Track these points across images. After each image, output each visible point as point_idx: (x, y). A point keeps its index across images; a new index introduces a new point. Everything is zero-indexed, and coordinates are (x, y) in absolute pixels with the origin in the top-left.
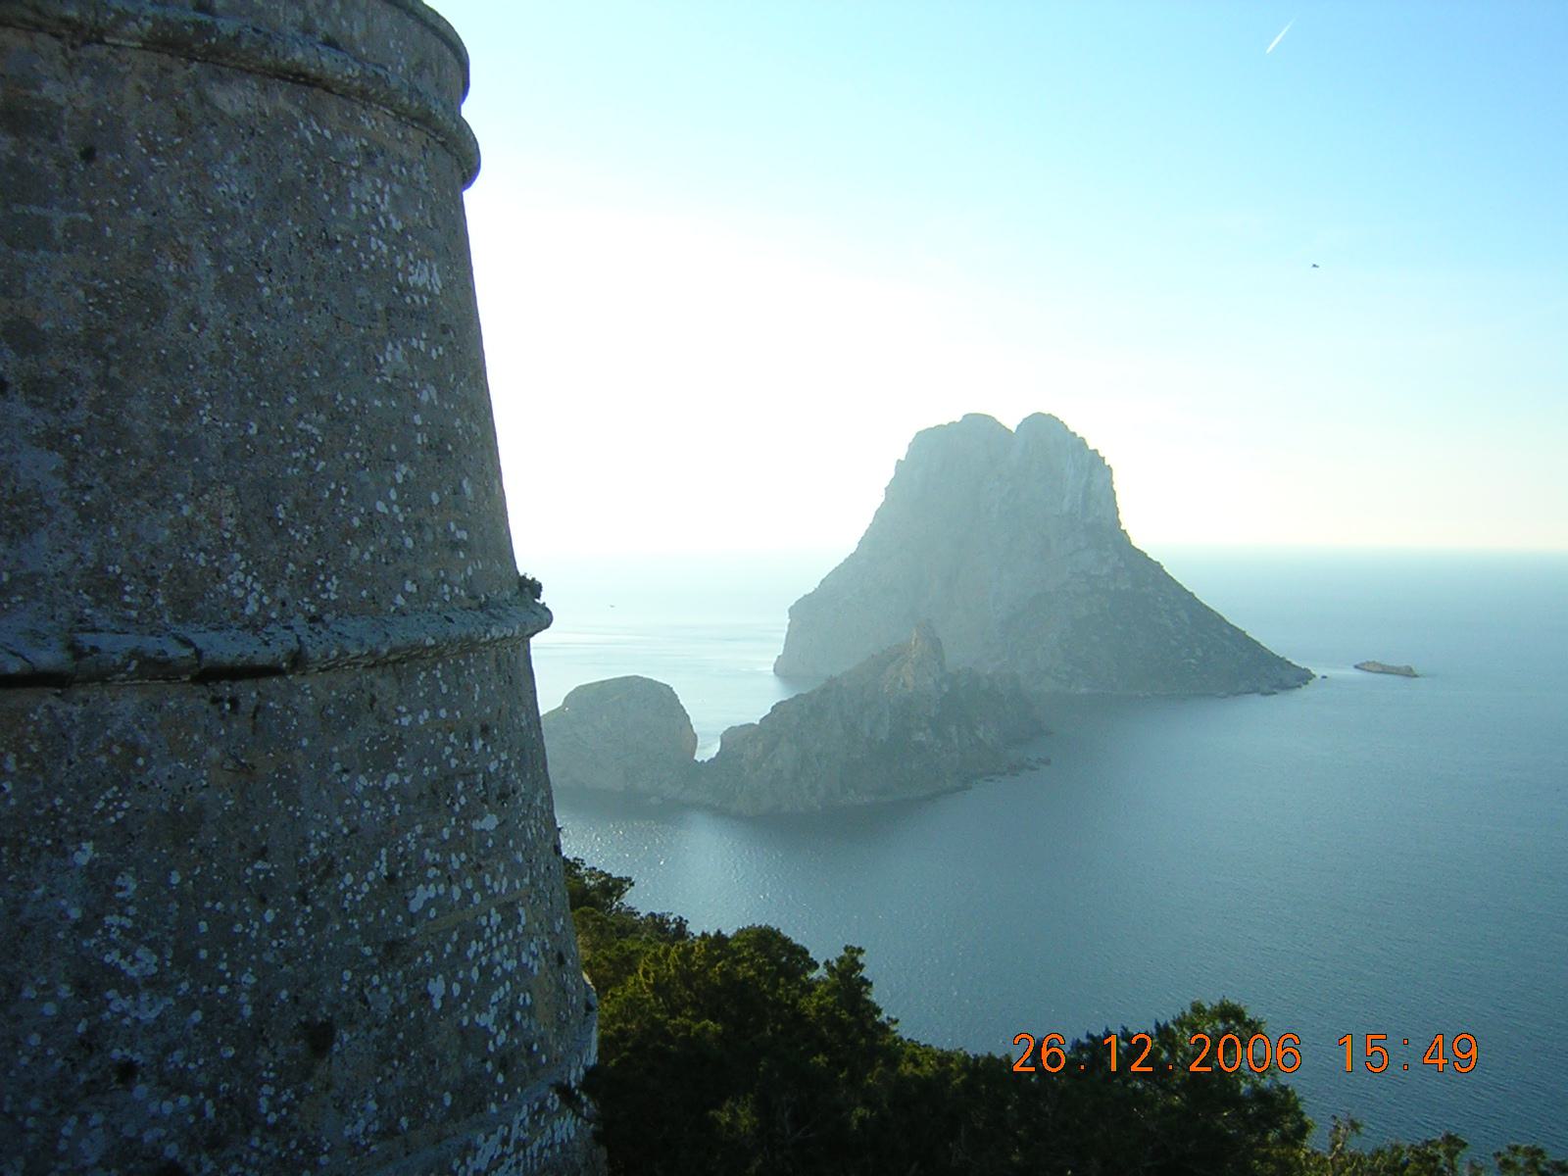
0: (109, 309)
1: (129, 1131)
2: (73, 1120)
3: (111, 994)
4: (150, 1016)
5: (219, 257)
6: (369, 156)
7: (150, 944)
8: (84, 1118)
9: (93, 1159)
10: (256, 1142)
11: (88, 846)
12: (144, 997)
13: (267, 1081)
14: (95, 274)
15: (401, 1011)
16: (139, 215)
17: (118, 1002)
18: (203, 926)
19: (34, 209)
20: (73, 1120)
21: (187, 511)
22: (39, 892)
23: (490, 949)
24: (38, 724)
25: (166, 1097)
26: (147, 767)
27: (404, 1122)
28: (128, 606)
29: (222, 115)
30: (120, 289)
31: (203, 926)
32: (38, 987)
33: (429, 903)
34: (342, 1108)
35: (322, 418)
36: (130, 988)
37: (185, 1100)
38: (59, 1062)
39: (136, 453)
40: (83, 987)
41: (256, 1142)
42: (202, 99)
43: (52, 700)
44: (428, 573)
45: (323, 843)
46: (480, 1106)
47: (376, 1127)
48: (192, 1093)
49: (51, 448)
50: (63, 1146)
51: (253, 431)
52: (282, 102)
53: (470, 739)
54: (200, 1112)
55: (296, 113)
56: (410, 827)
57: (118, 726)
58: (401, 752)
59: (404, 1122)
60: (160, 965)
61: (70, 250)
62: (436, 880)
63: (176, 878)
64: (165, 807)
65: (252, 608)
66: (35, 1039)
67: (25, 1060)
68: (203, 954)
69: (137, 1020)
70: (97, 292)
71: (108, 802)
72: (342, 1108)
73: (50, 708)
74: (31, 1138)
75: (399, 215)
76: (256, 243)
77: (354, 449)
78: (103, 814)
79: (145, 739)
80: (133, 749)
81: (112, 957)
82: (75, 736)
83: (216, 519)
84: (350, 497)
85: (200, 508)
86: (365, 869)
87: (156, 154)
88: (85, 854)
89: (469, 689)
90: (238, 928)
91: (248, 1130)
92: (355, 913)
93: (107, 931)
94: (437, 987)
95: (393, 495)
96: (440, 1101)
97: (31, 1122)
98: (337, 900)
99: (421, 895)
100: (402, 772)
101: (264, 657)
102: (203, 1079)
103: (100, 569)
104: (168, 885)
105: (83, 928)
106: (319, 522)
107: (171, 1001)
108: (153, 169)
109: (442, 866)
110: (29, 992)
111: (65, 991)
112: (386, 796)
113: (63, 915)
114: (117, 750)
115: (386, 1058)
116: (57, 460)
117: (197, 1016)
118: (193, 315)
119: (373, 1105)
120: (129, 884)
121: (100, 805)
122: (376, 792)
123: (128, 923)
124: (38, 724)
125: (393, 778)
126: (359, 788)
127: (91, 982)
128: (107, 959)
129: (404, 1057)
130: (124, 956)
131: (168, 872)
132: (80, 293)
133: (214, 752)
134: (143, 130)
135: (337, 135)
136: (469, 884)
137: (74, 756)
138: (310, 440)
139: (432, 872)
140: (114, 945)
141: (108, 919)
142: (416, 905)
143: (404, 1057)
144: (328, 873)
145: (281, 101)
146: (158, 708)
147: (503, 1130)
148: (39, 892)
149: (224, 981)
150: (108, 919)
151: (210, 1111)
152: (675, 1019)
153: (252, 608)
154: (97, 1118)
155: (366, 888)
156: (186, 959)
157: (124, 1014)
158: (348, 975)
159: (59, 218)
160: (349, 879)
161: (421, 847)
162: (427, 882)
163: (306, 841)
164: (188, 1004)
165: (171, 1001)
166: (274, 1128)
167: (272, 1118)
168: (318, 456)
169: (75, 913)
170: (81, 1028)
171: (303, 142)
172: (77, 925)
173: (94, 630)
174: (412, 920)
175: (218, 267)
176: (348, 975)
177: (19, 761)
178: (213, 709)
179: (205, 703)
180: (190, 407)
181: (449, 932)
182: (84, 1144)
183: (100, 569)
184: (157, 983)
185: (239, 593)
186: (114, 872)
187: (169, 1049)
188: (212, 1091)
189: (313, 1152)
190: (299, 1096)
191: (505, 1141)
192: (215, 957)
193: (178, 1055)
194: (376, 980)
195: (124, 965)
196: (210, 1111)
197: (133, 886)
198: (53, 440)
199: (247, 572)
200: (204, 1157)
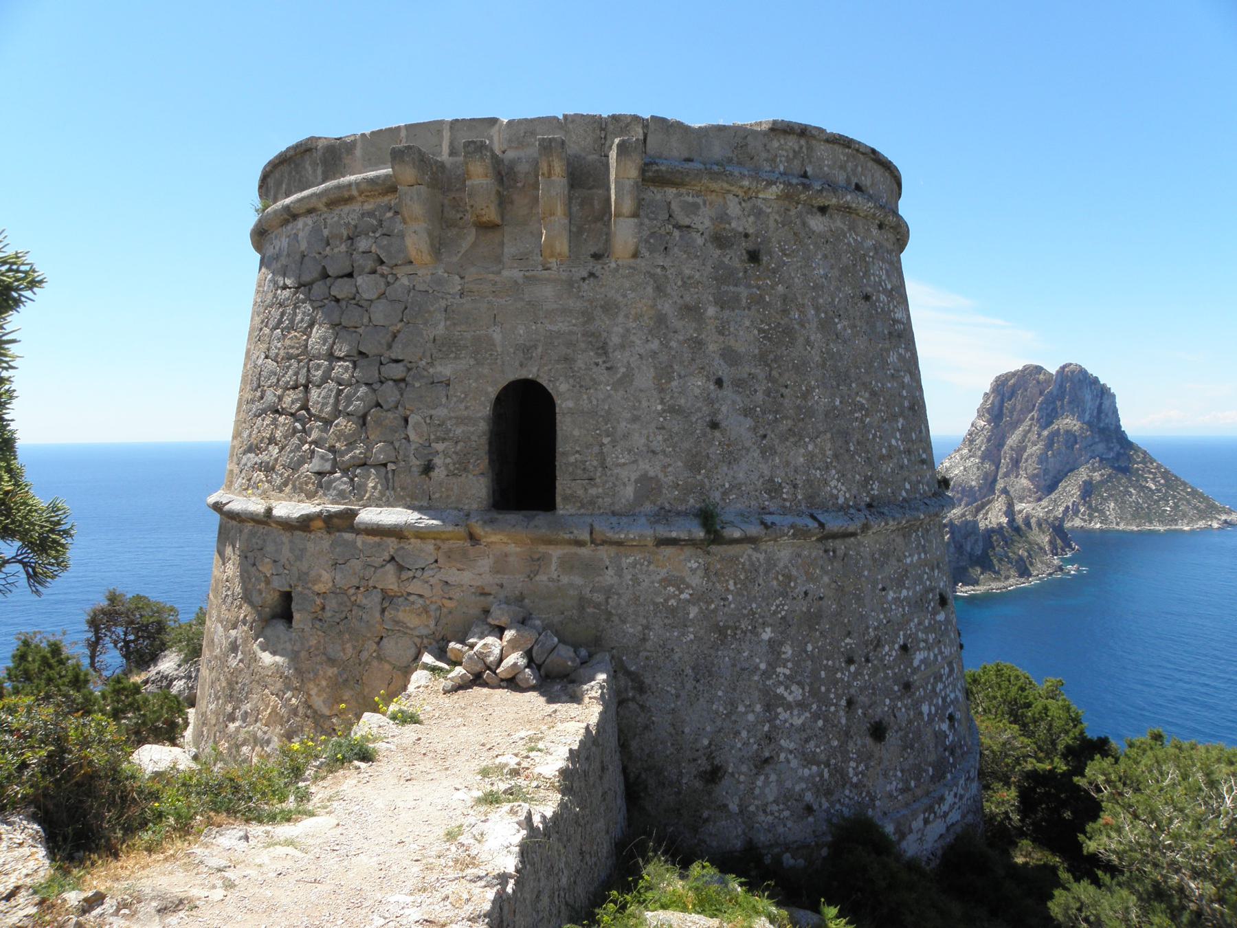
0: (770, 340)
1: (788, 784)
2: (762, 778)
3: (780, 710)
4: (798, 722)
5: (818, 309)
6: (875, 249)
7: (799, 683)
8: (767, 777)
9: (771, 799)
10: (847, 792)
11: (768, 630)
12: (796, 712)
13: (852, 759)
14: (762, 321)
15: (910, 722)
16: (780, 288)
17: (783, 715)
18: (823, 674)
19: (732, 288)
20: (762, 778)
21: (810, 447)
22: (745, 654)
23: (945, 687)
24: (743, 564)
25: (804, 767)
26: (795, 587)
27: (913, 784)
28: (785, 500)
29: (814, 232)
30: (774, 329)
31: (823, 674)
32: (746, 707)
33: (922, 661)
34: (885, 775)
35: (867, 395)
36: (789, 707)
37: (814, 768)
38: (755, 746)
39: (786, 418)
40: (768, 707)
41: (847, 792)
42: (804, 224)
43: (750, 551)
44: (914, 478)
45: (876, 629)
46: (943, 776)
47: (900, 786)
48: (818, 765)
49: (746, 416)
50: (757, 791)
51: (837, 403)
52: (839, 223)
53: (933, 570)
54: (821, 775)
55: (846, 228)
56: (912, 620)
57: (781, 565)
58: (907, 578)
59: (913, 784)
60: (803, 695)
61: (749, 309)
62: (924, 649)
63: (810, 648)
64: (804, 609)
65: (841, 501)
66: (744, 734)
67: (739, 745)
68: (823, 689)
69: (792, 725)
70: (764, 331)
71: (777, 606)
72: (885, 775)
73: (749, 556)
74: (742, 787)
75: (890, 282)
76: (833, 300)
77: (881, 411)
78: (775, 613)
79: (794, 572)
80: (789, 577)
81: (780, 690)
82: (761, 570)
83: (822, 450)
84: (881, 438)
85: (816, 446)
86: (894, 643)
87: (786, 255)
88: (767, 634)
89: (931, 542)
90: (839, 675)
91: (844, 786)
92: (889, 668)
93: (778, 676)
94: (925, 708)
95: (898, 435)
96: (926, 771)
97: (742, 778)
98: (882, 660)
99: (919, 657)
100: (908, 589)
101: (851, 529)
102: (823, 757)
103: (771, 480)
104: (806, 652)
105: (766, 674)
106: (868, 452)
107: (808, 715)
108: (785, 264)
109: (926, 641)
110: (741, 709)
111: (758, 708)
112: (902, 602)
113: (757, 668)
114: (780, 578)
115: (905, 749)
116: (749, 422)
117: (820, 723)
118: (808, 342)
119: (899, 774)
120: (788, 651)
121: (773, 608)
122: (897, 600)
123: (788, 672)
124: (743, 564)
125: (904, 592)
126: (890, 598)
127: (772, 703)
128: (778, 691)
129: (912, 747)
130: (786, 689)
131: (806, 644)
132: (756, 332)
133: (826, 579)
134: (779, 243)
135: (863, 238)
136: (936, 651)
137: (761, 581)
138: (862, 407)
139: (922, 645)
140: (781, 683)
141: (778, 670)
142: (916, 663)
143: (912, 747)
144: (877, 645)
145: (839, 223)
146: (799, 555)
147: (955, 789)
148: (745, 654)
149: (833, 704)
150: (778, 670)
151: (826, 775)
152: (318, 695)
153: (841, 501)
154: (773, 777)
155: (894, 653)
156: (814, 693)
157: (786, 721)
158: (887, 701)
159: (744, 292)
160: (887, 648)
161: (917, 631)
162: (920, 650)
163: (868, 628)
164: (816, 716)
165: (808, 715)
166: (856, 786)
167: (855, 780)
168: (866, 416)
169: (763, 666)
170: (766, 728)
171: (849, 244)
172: (764, 673)
173: (771, 513)
174: (916, 670)
175: (817, 314)
176: (887, 701)
177: (735, 584)
178: (825, 556)
179: (821, 552)
180: (810, 391)
181: (929, 677)
182: (767, 790)
183: (771, 480)
184: (802, 705)
185: (835, 492)
186: (781, 644)
187: (807, 741)
188: (828, 765)
189: (873, 800)
190: (867, 768)
191: (955, 796)
192: (828, 690)
193: (812, 744)
194: (899, 704)
195: (786, 694)
196: (826, 775)
197: (790, 652)
198: (747, 412)
199: (838, 480)
200: (824, 800)
